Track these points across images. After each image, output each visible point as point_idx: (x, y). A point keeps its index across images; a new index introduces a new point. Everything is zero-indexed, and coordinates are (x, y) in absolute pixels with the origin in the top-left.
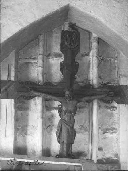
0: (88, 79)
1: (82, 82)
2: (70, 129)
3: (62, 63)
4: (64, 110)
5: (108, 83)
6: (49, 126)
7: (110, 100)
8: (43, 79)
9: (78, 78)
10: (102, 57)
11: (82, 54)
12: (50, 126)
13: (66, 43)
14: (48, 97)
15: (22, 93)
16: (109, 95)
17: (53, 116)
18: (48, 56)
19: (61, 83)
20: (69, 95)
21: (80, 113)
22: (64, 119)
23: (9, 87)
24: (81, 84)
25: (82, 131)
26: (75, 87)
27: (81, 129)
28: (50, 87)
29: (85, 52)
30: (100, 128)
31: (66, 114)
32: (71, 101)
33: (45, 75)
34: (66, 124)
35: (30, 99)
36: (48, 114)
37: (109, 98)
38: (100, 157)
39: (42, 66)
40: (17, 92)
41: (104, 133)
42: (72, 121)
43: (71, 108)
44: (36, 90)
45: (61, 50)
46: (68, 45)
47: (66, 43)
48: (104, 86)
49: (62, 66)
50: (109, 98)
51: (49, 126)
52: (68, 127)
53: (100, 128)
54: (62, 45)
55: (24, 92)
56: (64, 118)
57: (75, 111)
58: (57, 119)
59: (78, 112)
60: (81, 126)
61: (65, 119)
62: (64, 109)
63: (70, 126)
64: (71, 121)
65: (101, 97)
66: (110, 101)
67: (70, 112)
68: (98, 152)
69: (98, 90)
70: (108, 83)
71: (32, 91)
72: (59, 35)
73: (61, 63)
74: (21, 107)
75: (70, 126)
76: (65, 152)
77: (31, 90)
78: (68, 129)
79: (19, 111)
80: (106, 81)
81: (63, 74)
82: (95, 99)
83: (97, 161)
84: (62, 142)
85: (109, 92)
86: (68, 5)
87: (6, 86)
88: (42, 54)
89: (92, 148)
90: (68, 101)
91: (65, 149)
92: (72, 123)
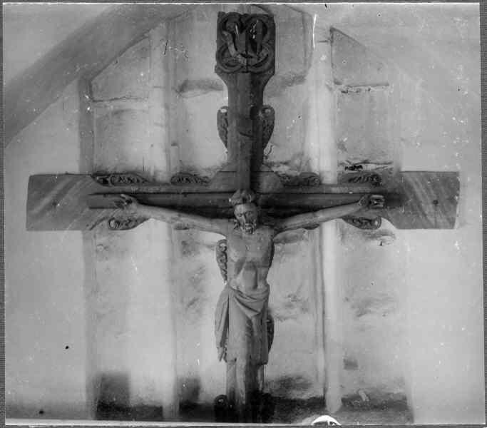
0: (306, 155)
1: (286, 163)
2: (254, 320)
3: (224, 111)
4: (232, 261)
5: (366, 162)
6: (192, 303)
7: (374, 217)
8: (169, 162)
9: (278, 153)
10: (343, 86)
11: (283, 78)
12: (196, 302)
13: (232, 49)
14: (182, 221)
15: (105, 211)
16: (369, 204)
17: (201, 270)
18: (183, 88)
19: (223, 172)
20: (247, 215)
21: (284, 257)
22: (235, 287)
23: (61, 194)
24: (284, 169)
25: (296, 311)
26: (266, 184)
27: (289, 306)
28: (186, 188)
29: (295, 71)
30: (347, 300)
31: (242, 271)
32: (257, 232)
33: (173, 149)
34: (243, 304)
35: (128, 228)
36: (190, 264)
37: (371, 211)
38: (350, 390)
39: (163, 123)
40: (87, 209)
41: (360, 316)
42: (258, 294)
43: (255, 254)
44: (144, 200)
45: (219, 71)
46: (239, 56)
47: (232, 49)
48: (354, 173)
49: (223, 120)
50: (370, 214)
51: (192, 303)
52: (250, 315)
53: (347, 300)
54: (222, 54)
55: (107, 208)
56: (235, 283)
57: (269, 259)
58: (216, 285)
59: (278, 256)
60: (289, 296)
61: (238, 287)
62: (233, 255)
63: (256, 311)
64: (256, 292)
65: (349, 210)
66: (374, 221)
67: (253, 266)
68: (346, 372)
69: (334, 190)
70: (366, 162)
71: (134, 206)
72: (212, 25)
73: (219, 111)
74: (105, 248)
75: (256, 311)
76: (242, 391)
77: (129, 202)
78: (249, 321)
79: (100, 261)
80: (360, 156)
81: (229, 143)
82: (328, 220)
83: (343, 400)
84: (232, 361)
85: (369, 197)
86: (456, 174)
87: (54, 192)
88: (160, 87)
89: (326, 360)
90: (243, 231)
91: (241, 378)
92: (258, 300)
